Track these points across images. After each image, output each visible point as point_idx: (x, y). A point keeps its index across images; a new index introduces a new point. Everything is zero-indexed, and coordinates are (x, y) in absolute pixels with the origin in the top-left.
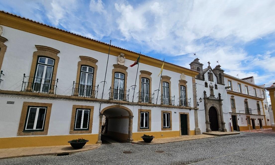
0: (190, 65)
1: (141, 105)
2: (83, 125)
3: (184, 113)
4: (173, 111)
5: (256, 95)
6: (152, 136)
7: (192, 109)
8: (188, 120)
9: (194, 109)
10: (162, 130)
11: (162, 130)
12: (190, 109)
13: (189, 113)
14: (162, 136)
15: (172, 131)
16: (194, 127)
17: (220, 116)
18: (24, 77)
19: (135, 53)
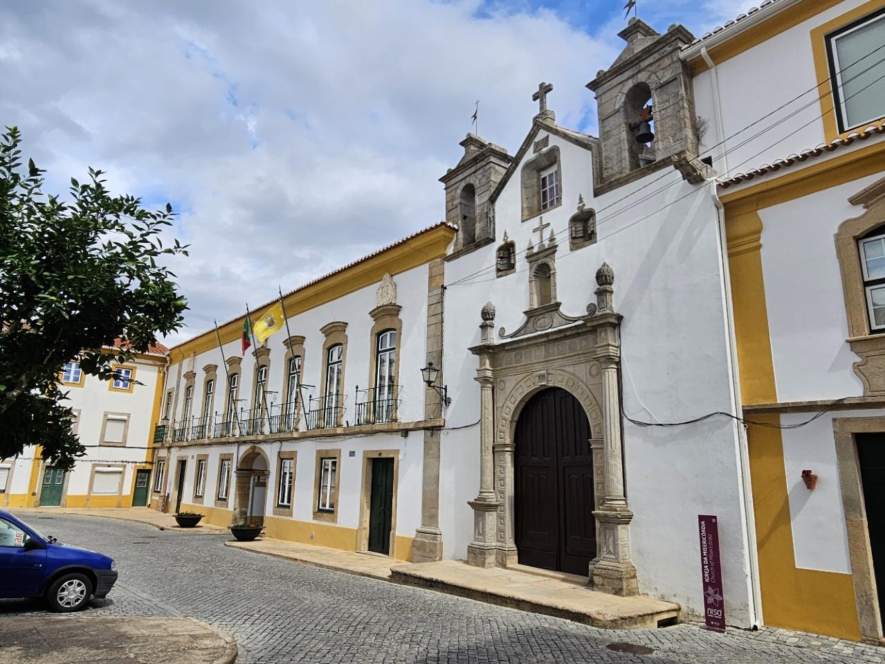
0: (443, 185)
1: (281, 440)
2: (880, 607)
3: (380, 454)
4: (344, 446)
5: (816, 101)
6: (199, 515)
7: (411, 430)
8: (366, 483)
9: (426, 429)
10: (314, 519)
11: (314, 519)
12: (405, 432)
13: (397, 451)
14: (312, 538)
15: (338, 526)
16: (418, 525)
17: (333, 440)
18: (67, 398)
19: (384, 250)
